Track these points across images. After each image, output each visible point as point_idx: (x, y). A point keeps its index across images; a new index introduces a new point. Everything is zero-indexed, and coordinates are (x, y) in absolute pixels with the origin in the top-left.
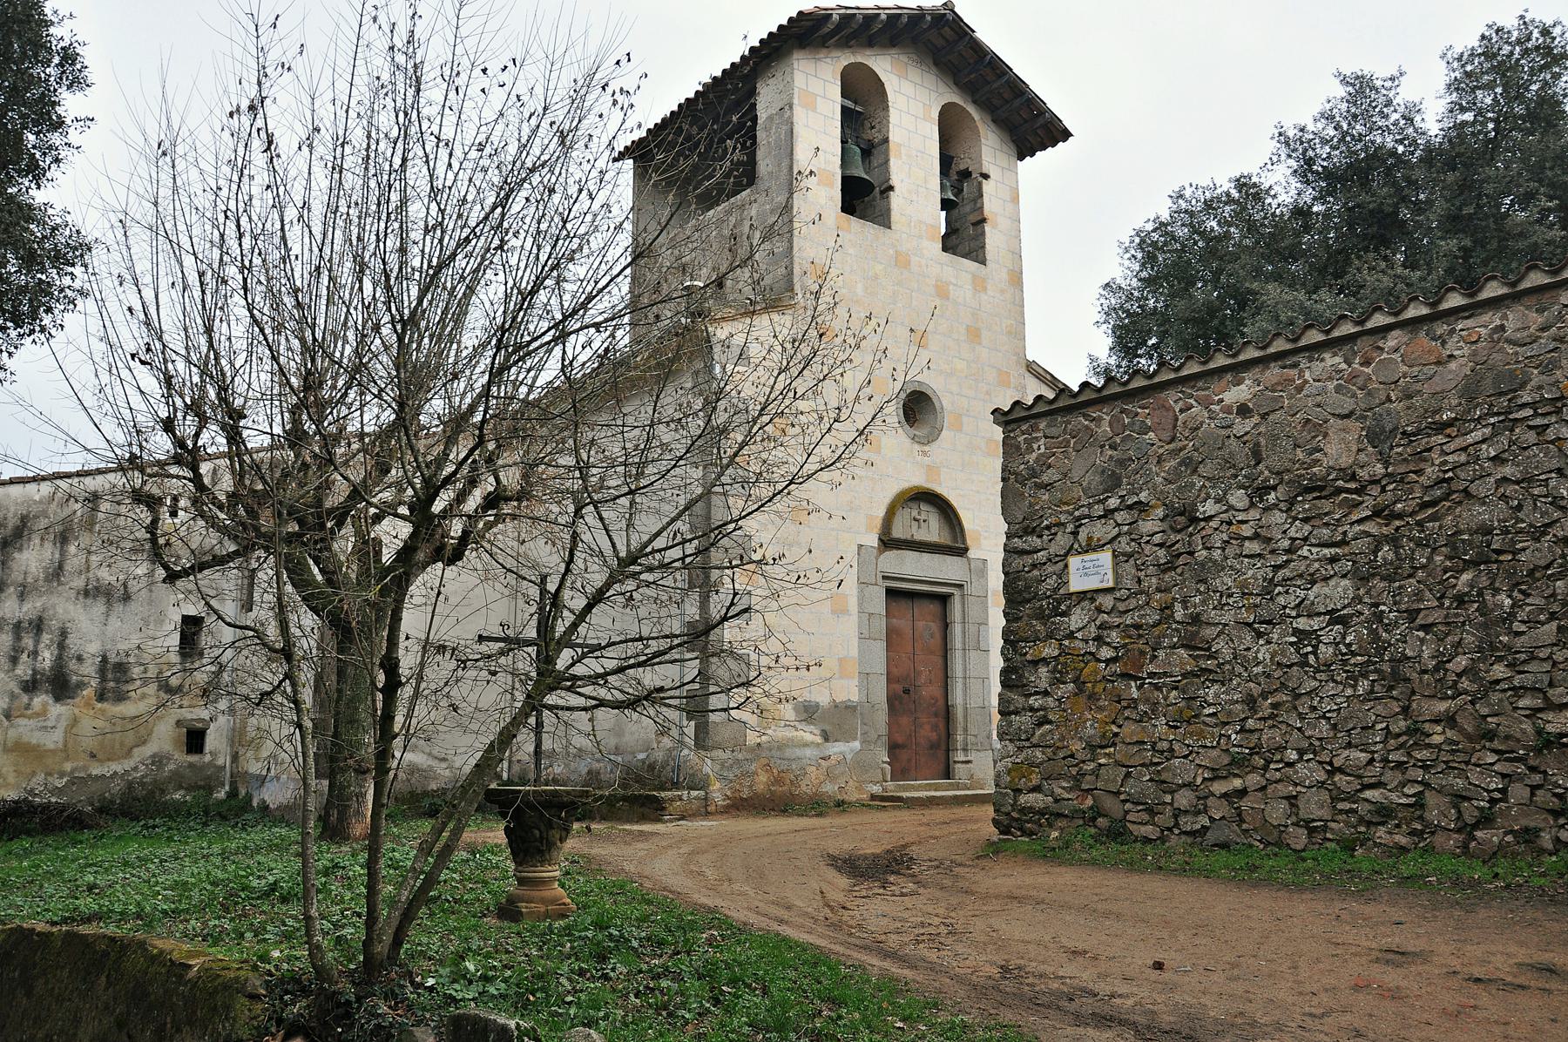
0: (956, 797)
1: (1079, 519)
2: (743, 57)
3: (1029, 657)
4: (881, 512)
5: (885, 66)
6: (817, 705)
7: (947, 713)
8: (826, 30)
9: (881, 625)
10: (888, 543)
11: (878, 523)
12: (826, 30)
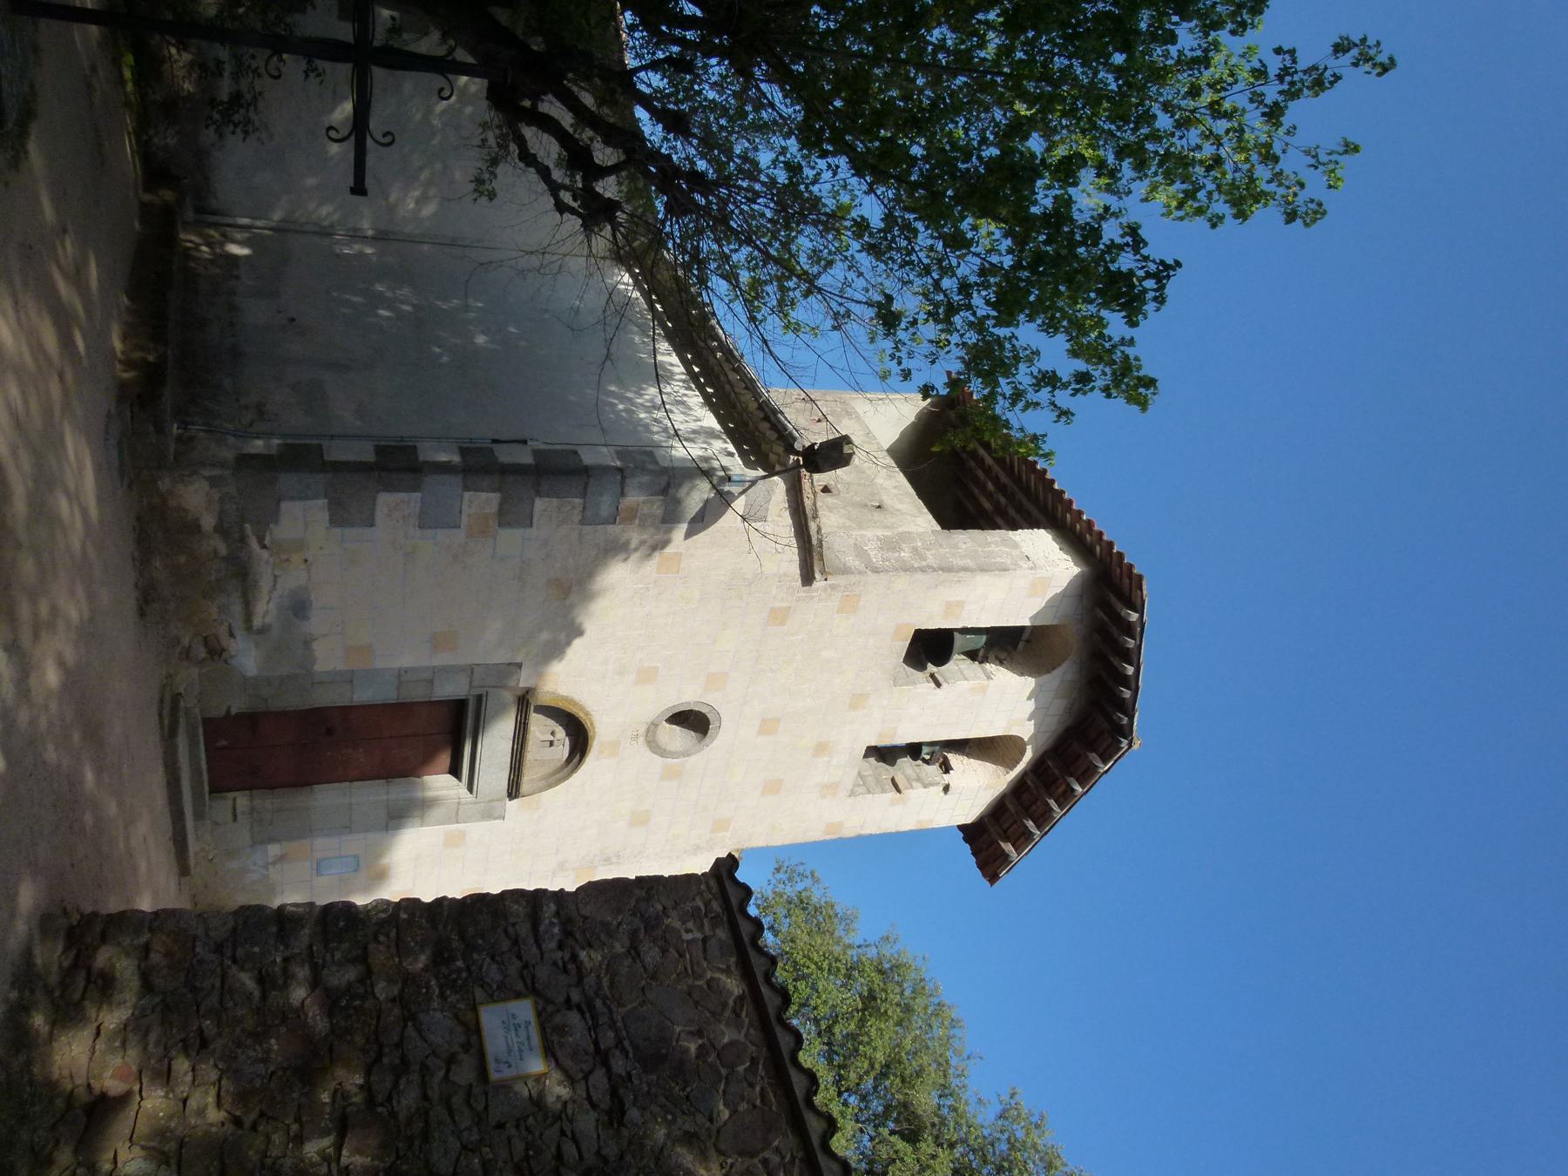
0: (202, 783)
1: (591, 1007)
3: (372, 947)
6: (306, 618)
8: (1118, 606)
9: (417, 694)
12: (1118, 606)
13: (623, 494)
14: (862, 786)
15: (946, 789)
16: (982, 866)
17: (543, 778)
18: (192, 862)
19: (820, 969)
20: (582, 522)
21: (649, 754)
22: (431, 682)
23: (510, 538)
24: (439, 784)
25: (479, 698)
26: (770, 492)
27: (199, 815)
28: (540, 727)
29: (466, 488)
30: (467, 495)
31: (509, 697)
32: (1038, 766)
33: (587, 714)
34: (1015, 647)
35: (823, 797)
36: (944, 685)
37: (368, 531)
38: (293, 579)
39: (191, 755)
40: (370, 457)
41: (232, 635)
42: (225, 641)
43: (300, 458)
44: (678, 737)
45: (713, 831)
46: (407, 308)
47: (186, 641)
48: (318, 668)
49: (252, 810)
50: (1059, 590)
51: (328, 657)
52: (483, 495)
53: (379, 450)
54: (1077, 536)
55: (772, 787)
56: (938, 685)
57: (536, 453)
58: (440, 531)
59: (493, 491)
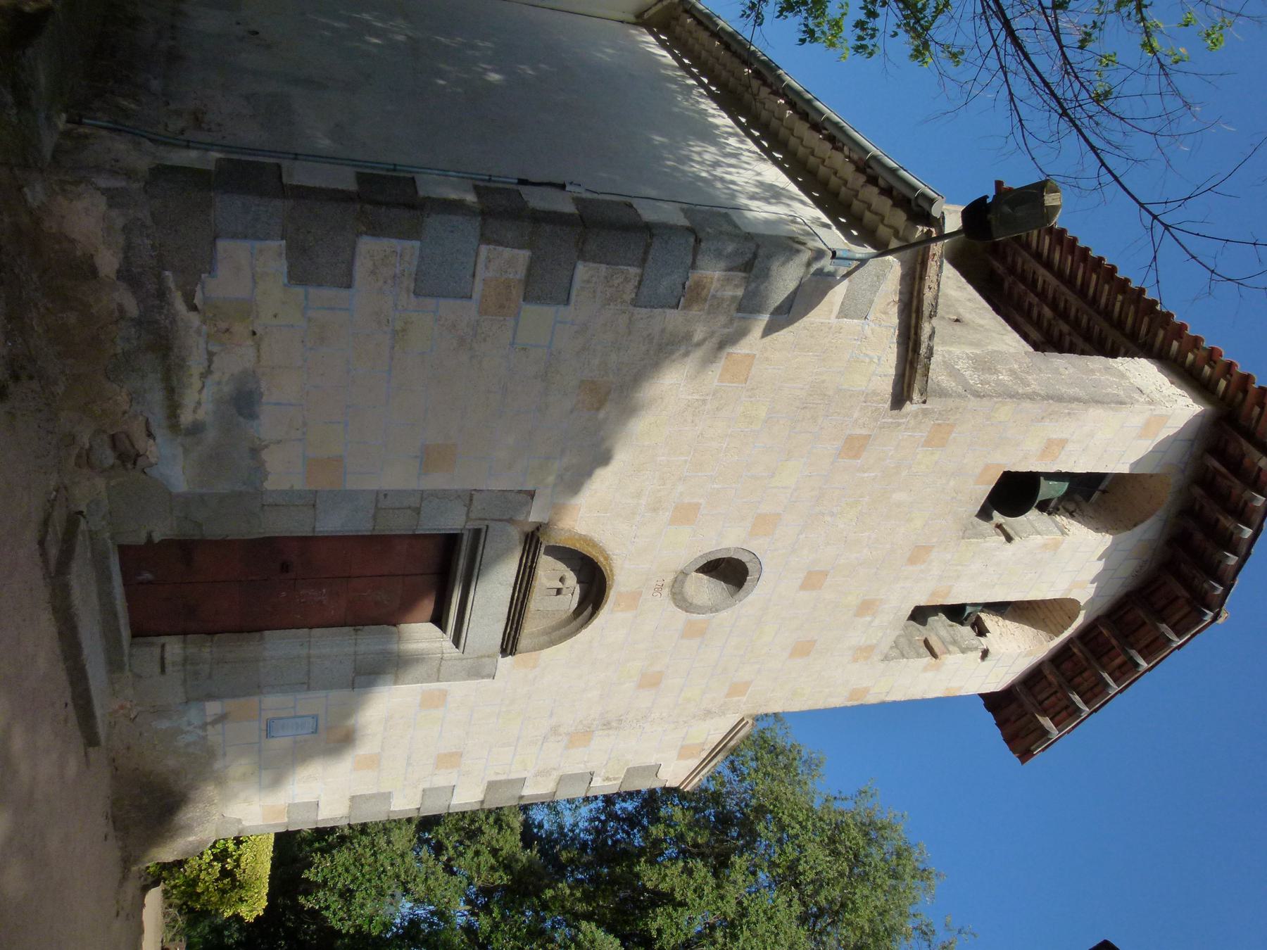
2: (1182, 327)
6: (253, 416)
7: (260, 630)
9: (398, 524)
13: (693, 266)
14: (900, 650)
15: (985, 654)
16: (1010, 740)
17: (546, 632)
18: (102, 730)
19: (804, 828)
20: (635, 303)
21: (672, 607)
22: (417, 511)
23: (537, 316)
24: (420, 635)
25: (477, 533)
26: (880, 277)
27: (115, 664)
28: (549, 571)
29: (484, 239)
30: (484, 249)
31: (515, 534)
32: (1085, 635)
33: (607, 558)
34: (1088, 498)
35: (855, 660)
36: (1017, 539)
37: (344, 293)
38: (235, 360)
39: (95, 596)
40: (351, 185)
41: (150, 435)
42: (141, 443)
43: (250, 177)
44: (705, 589)
45: (728, 695)
46: (401, 38)
47: (85, 440)
48: (269, 485)
49: (185, 661)
50: (1172, 432)
51: (284, 472)
52: (507, 252)
53: (362, 178)
54: (1189, 369)
55: (802, 649)
56: (1009, 539)
57: (578, 201)
58: (442, 302)
59: (521, 247)
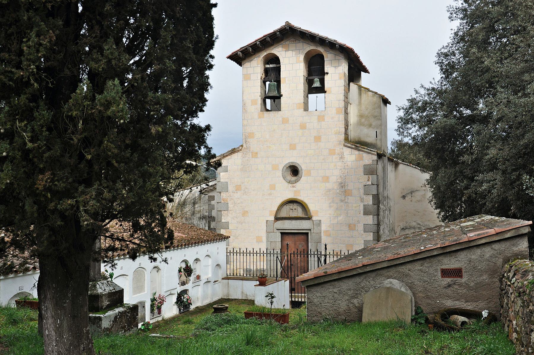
4: (276, 209)
5: (278, 51)
10: (277, 219)
11: (274, 215)
